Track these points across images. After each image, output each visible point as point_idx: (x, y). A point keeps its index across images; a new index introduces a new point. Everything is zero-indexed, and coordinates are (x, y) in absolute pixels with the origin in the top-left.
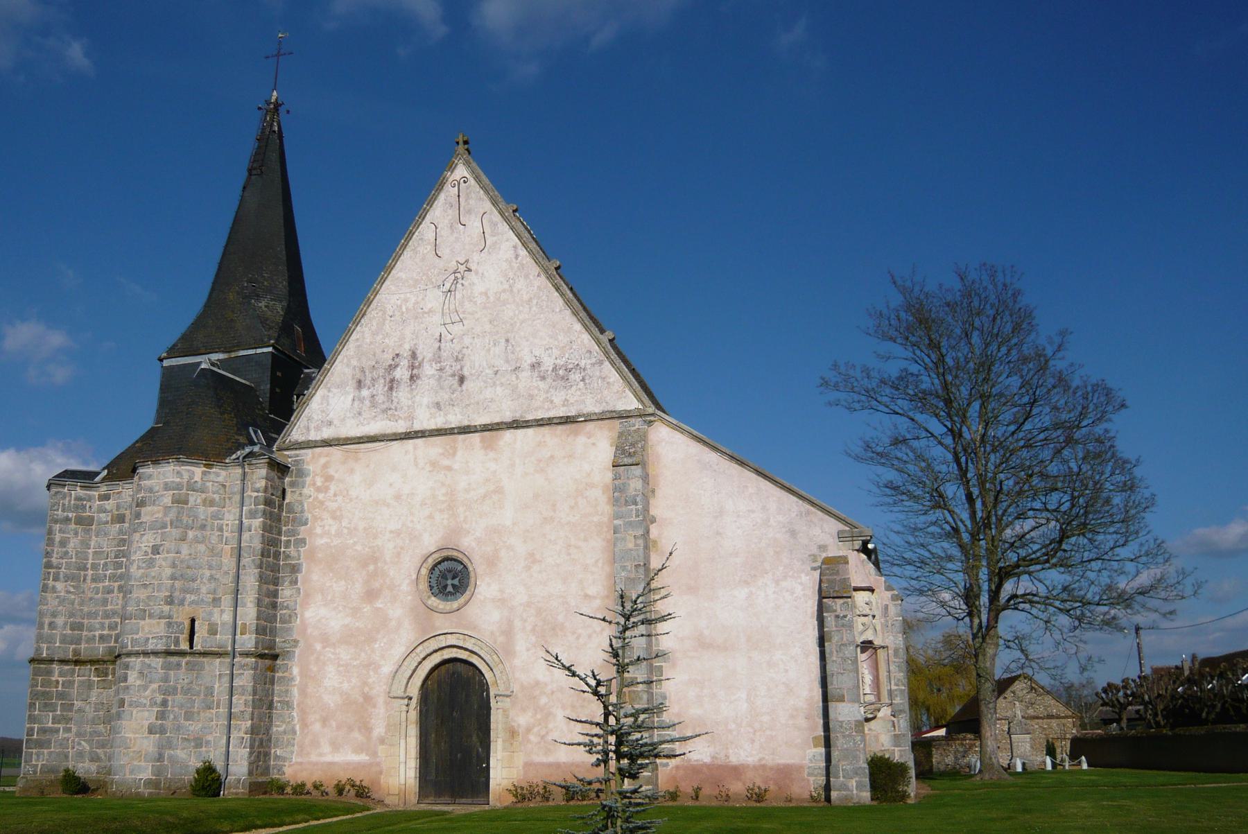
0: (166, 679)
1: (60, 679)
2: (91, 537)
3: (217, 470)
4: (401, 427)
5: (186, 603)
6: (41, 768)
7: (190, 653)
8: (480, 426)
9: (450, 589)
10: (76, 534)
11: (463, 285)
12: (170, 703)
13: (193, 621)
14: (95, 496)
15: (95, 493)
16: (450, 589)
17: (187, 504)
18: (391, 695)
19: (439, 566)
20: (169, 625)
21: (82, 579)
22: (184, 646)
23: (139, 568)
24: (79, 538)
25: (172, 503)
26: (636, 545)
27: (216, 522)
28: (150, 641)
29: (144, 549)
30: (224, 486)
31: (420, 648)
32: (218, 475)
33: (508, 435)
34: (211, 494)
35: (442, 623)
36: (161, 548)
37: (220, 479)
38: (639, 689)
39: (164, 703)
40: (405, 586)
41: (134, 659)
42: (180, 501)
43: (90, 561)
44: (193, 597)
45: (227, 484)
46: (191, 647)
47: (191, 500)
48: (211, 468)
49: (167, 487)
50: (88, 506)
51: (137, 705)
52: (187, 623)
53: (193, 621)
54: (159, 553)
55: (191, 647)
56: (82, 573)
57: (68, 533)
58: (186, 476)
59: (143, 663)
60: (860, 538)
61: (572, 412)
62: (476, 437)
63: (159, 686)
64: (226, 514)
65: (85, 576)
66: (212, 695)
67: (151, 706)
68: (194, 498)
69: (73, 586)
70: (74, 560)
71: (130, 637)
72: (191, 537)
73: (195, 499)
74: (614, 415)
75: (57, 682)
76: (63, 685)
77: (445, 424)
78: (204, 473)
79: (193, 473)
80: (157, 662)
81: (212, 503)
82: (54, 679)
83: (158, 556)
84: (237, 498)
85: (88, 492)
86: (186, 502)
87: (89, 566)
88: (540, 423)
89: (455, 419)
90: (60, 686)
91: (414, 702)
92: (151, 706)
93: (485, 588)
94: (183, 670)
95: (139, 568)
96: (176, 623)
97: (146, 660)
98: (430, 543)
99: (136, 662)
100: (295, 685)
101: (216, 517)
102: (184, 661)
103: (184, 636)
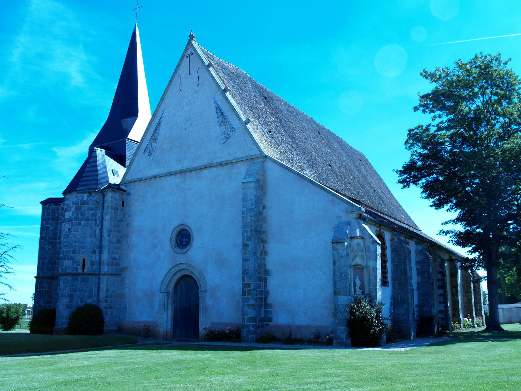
0: (73, 286)
1: (47, 285)
2: (58, 226)
3: (94, 195)
4: (165, 171)
5: (81, 252)
6: (269, 311)
7: (83, 274)
8: (195, 167)
9: (184, 243)
10: (52, 225)
11: (190, 103)
12: (74, 296)
13: (84, 260)
14: (59, 208)
15: (59, 207)
16: (184, 243)
17: (81, 210)
18: (161, 291)
19: (181, 233)
20: (74, 262)
21: (55, 243)
22: (80, 271)
23: (64, 238)
24: (53, 226)
25: (75, 210)
26: (251, 220)
27: (93, 217)
28: (68, 269)
29: (66, 230)
30: (97, 201)
31: (172, 270)
32: (94, 197)
33: (206, 171)
34: (91, 206)
35: (180, 259)
36: (71, 230)
37: (95, 199)
38: (251, 289)
39: (72, 296)
40: (167, 244)
41: (62, 277)
42: (78, 209)
43: (58, 236)
44: (84, 250)
45: (98, 201)
46: (83, 271)
47: (83, 208)
48: (91, 194)
49: (74, 203)
50: (57, 212)
51: (63, 296)
52: (81, 261)
53: (84, 260)
54: (70, 232)
55: (83, 271)
56: (55, 241)
57: (49, 225)
58: (80, 198)
59: (65, 278)
60: (356, 212)
61: (231, 158)
62: (194, 173)
63: (70, 288)
64: (98, 214)
65: (56, 242)
66: (92, 291)
67: (67, 297)
68: (84, 207)
69: (51, 247)
70: (51, 235)
71: (61, 267)
72: (83, 224)
73: (85, 207)
74: (249, 158)
75: (45, 286)
76: (48, 287)
77: (182, 168)
78: (88, 197)
79: (83, 197)
80: (69, 278)
81: (92, 209)
82: (44, 285)
83: (70, 233)
84: (101, 207)
85: (57, 207)
86: (80, 209)
87: (58, 238)
88: (221, 164)
89: (186, 165)
90: (47, 288)
91: (171, 294)
92: (67, 297)
93: (197, 242)
94: (80, 281)
95: (64, 238)
96: (77, 261)
97: (66, 277)
98: (175, 223)
99: (62, 278)
100: (126, 287)
101: (93, 215)
102: (80, 278)
103: (80, 266)
